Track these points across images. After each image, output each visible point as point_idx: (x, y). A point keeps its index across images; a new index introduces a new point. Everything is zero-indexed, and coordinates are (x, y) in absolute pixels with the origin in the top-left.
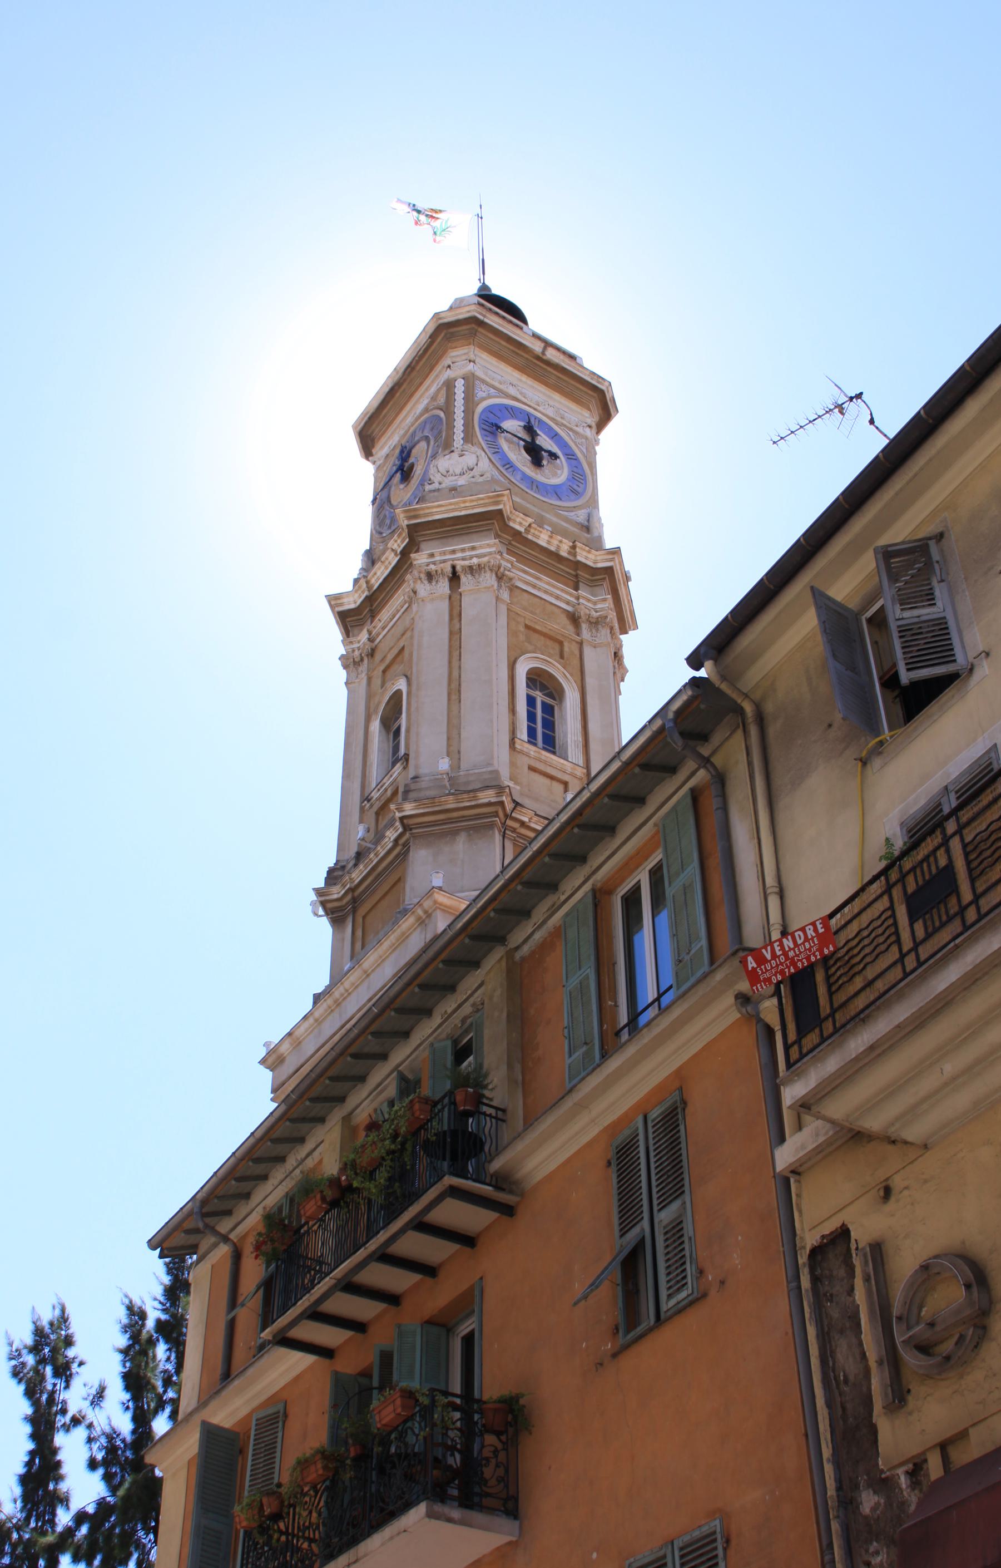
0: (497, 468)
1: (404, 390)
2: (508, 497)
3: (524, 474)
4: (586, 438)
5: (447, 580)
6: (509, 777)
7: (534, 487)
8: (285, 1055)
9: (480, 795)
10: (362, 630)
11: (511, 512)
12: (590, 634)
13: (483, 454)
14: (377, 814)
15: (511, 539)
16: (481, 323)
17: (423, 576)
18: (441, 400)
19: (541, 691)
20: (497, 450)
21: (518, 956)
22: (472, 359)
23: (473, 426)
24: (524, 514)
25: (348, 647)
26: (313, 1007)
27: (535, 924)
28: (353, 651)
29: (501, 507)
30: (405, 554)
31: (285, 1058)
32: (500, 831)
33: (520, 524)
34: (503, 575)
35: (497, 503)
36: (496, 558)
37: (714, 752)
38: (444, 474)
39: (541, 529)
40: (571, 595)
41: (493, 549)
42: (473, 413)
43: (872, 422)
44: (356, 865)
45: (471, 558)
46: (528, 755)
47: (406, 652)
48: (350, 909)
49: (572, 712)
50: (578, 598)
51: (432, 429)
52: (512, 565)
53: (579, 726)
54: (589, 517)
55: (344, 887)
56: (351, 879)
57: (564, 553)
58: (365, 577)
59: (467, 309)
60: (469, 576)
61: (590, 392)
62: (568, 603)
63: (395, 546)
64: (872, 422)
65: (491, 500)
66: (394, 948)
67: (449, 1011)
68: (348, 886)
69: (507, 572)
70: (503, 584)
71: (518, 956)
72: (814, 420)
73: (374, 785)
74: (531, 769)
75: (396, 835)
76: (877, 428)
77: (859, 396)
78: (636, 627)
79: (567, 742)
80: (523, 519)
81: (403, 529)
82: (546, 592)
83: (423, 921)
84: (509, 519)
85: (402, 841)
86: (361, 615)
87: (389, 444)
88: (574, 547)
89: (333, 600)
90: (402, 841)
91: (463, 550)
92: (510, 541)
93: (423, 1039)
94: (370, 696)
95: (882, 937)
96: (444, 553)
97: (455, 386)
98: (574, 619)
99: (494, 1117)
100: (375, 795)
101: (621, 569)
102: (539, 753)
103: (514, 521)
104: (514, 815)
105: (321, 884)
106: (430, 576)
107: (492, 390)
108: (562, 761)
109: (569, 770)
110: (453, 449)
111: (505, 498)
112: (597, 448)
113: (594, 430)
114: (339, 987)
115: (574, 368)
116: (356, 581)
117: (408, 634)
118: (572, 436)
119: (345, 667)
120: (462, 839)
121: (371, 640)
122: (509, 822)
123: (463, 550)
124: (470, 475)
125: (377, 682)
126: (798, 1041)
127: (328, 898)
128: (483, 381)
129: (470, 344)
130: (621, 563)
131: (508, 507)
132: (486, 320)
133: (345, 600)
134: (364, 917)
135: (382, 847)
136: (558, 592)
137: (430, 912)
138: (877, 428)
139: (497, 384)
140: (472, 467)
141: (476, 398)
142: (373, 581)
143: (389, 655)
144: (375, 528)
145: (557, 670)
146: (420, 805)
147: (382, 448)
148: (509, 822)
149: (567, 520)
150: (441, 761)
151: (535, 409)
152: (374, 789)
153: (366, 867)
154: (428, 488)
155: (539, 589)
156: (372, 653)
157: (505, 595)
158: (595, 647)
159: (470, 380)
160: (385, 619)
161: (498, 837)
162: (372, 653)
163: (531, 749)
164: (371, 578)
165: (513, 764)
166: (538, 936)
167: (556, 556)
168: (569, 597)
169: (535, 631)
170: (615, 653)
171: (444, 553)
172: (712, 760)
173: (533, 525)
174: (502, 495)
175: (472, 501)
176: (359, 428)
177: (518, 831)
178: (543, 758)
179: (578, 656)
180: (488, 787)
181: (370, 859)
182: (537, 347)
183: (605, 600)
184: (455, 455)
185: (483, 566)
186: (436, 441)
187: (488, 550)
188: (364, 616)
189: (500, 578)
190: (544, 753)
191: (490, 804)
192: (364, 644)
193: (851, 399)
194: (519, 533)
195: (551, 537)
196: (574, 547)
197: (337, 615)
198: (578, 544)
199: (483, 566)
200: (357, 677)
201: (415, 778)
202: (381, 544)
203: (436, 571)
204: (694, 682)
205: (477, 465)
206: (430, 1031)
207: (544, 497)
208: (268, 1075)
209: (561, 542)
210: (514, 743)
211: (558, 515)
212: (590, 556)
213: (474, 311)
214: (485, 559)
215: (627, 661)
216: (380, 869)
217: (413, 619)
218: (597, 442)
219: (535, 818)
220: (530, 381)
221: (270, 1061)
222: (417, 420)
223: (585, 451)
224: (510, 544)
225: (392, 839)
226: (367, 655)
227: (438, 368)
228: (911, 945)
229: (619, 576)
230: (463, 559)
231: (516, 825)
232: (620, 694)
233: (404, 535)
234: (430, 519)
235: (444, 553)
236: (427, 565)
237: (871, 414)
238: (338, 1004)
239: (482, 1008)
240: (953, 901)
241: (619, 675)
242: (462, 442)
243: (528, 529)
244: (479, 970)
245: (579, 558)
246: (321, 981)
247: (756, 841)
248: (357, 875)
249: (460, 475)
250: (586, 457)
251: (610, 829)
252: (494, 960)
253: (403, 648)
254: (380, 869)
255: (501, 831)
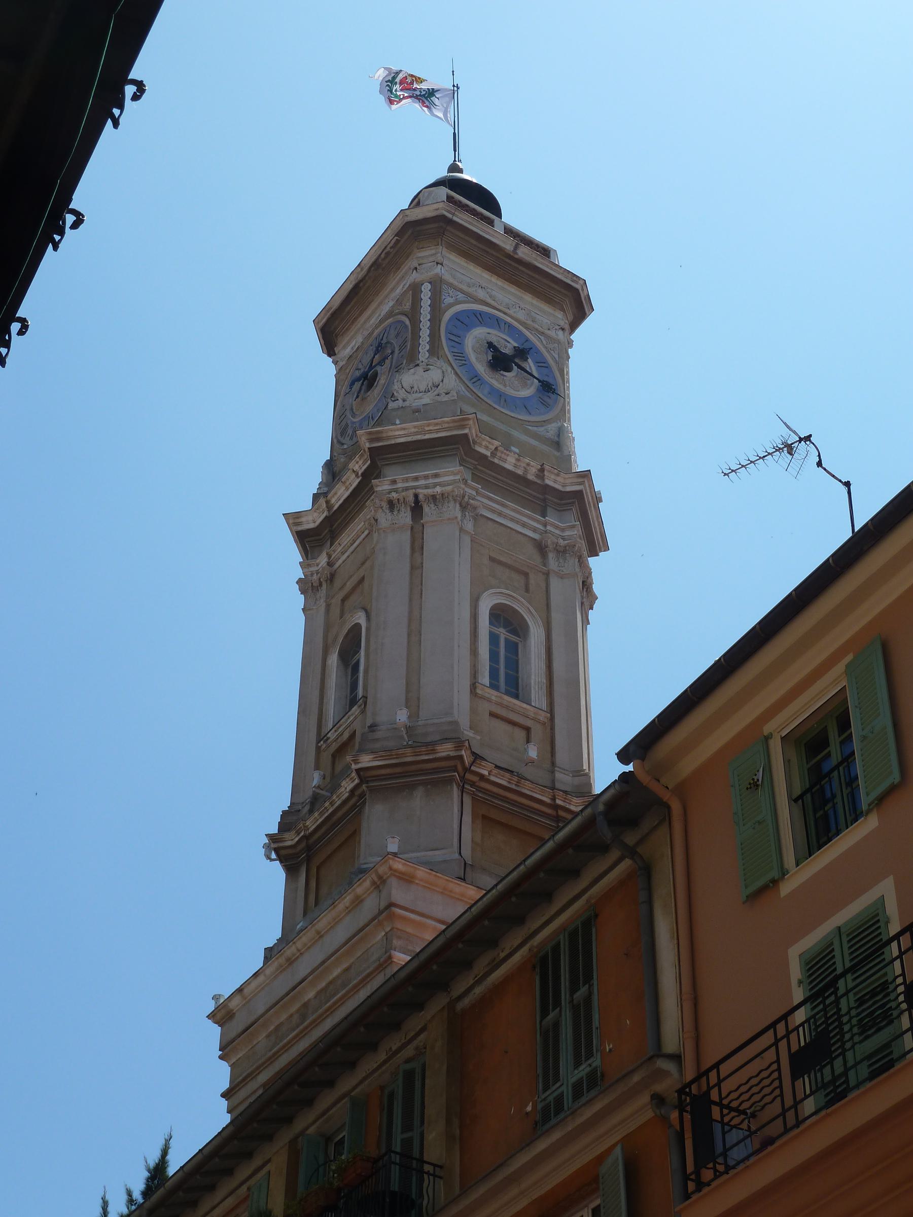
0: (464, 382)
1: (346, 705)
2: (473, 420)
3: (491, 386)
4: (559, 342)
5: (409, 509)
6: (469, 726)
7: (502, 400)
8: (234, 1011)
9: (438, 748)
10: (320, 552)
11: (476, 435)
12: (557, 563)
13: (450, 369)
14: (334, 756)
15: (476, 463)
16: (450, 222)
17: (385, 505)
18: (407, 306)
19: (505, 627)
20: (464, 362)
21: (460, 1006)
22: (440, 262)
23: (440, 337)
24: (489, 437)
25: (306, 570)
26: (265, 963)
27: (476, 977)
28: (312, 575)
29: (466, 431)
30: (368, 476)
31: (234, 1014)
32: (458, 785)
33: (487, 448)
34: (468, 504)
35: (463, 427)
36: (460, 487)
37: (641, 842)
38: (408, 391)
39: (508, 452)
40: (538, 521)
41: (458, 477)
42: (440, 321)
43: (819, 464)
44: (311, 811)
45: (435, 485)
46: (489, 700)
47: (366, 583)
48: (304, 857)
49: (536, 649)
50: (545, 525)
51: (397, 336)
52: (476, 492)
53: (543, 666)
54: (559, 431)
55: (299, 834)
56: (304, 827)
57: (531, 477)
58: (325, 494)
59: (436, 206)
60: (432, 505)
61: (563, 290)
62: (535, 530)
63: (356, 468)
64: (819, 464)
65: (456, 424)
66: (349, 910)
67: (394, 1048)
68: (302, 834)
69: (472, 501)
70: (467, 513)
71: (460, 1006)
72: (764, 457)
73: (330, 725)
74: (493, 715)
75: (352, 785)
76: (825, 469)
77: (808, 438)
78: (607, 548)
79: (530, 683)
80: (489, 442)
81: (364, 451)
82: (512, 519)
83: (378, 887)
84: (475, 442)
85: (357, 793)
86: (320, 535)
87: (349, 345)
88: (542, 470)
89: (293, 519)
90: (357, 793)
91: (426, 477)
92: (476, 465)
93: (368, 1072)
94: (328, 627)
95: (766, 1102)
96: (407, 479)
97: (422, 292)
98: (541, 548)
99: (432, 1175)
100: (332, 736)
101: (591, 492)
102: (501, 697)
103: (480, 445)
104: (473, 768)
105: (274, 830)
106: (391, 505)
107: (461, 295)
108: (525, 706)
109: (532, 715)
110: (418, 362)
111: (471, 422)
112: (570, 351)
113: (567, 332)
114: (291, 946)
115: (547, 266)
116: (316, 497)
117: (368, 564)
118: (544, 342)
119: (303, 591)
120: (419, 793)
121: (330, 564)
122: (468, 776)
123: (426, 477)
124: (436, 393)
125: (335, 611)
126: (697, 1172)
127: (281, 845)
128: (451, 285)
129: (438, 245)
130: (592, 486)
131: (474, 431)
132: (455, 219)
133: (303, 519)
134: (318, 868)
135: (337, 797)
136: (525, 519)
137: (384, 878)
138: (825, 469)
139: (464, 288)
140: (437, 384)
141: (443, 305)
142: (333, 501)
143: (348, 583)
144: (336, 437)
145: (522, 607)
146: (377, 757)
147: (344, 347)
148: (468, 776)
149: (536, 436)
150: (399, 712)
151: (505, 313)
152: (331, 730)
153: (321, 814)
154: (392, 405)
155: (505, 516)
156: (332, 578)
157: (469, 526)
158: (562, 578)
159: (437, 284)
160: (346, 542)
161: (456, 791)
162: (332, 578)
163: (493, 694)
164: (331, 498)
165: (473, 711)
166: (478, 990)
167: (522, 480)
168: (535, 524)
169: (500, 563)
170: (583, 582)
171: (407, 479)
172: (638, 850)
173: (500, 448)
174: (468, 419)
175: (437, 424)
176: (321, 324)
177: (477, 784)
178: (505, 703)
179: (544, 588)
180: (446, 740)
181: (326, 808)
182: (508, 244)
183: (573, 527)
184: (420, 370)
185: (446, 495)
186: (400, 350)
187: (452, 478)
188: (323, 538)
189: (464, 507)
190: (506, 698)
191: (448, 758)
192: (323, 568)
193: (801, 440)
194: (485, 457)
195: (518, 460)
196: (542, 470)
197: (295, 534)
198: (547, 467)
199: (446, 495)
200: (315, 603)
201: (373, 727)
202: (343, 456)
203: (398, 499)
204: (624, 776)
205: (442, 381)
206: (375, 1066)
207: (512, 411)
208: (217, 1030)
209: (528, 465)
210: (475, 688)
211: (527, 433)
212: (559, 479)
213: (443, 209)
214: (449, 488)
215: (596, 588)
216: (335, 818)
217: (373, 548)
218: (570, 344)
219: (495, 771)
220: (500, 282)
221: (219, 1016)
222: (381, 322)
223: (556, 356)
224: (476, 468)
225: (348, 790)
226: (326, 581)
227: (404, 269)
228: (792, 1103)
229: (588, 498)
230: (427, 487)
231: (475, 779)
232: (589, 623)
233: (366, 457)
234: (393, 442)
235: (406, 480)
236: (390, 493)
237: (819, 456)
238: (291, 962)
239: (425, 1052)
240: (827, 1071)
241: (587, 604)
242: (427, 354)
243: (495, 452)
244: (423, 1012)
245: (548, 482)
246: (273, 933)
247: (676, 942)
248: (311, 824)
249: (425, 392)
250: (557, 362)
251: (548, 896)
252: (438, 1003)
253: (363, 578)
254: (335, 818)
255: (459, 785)
